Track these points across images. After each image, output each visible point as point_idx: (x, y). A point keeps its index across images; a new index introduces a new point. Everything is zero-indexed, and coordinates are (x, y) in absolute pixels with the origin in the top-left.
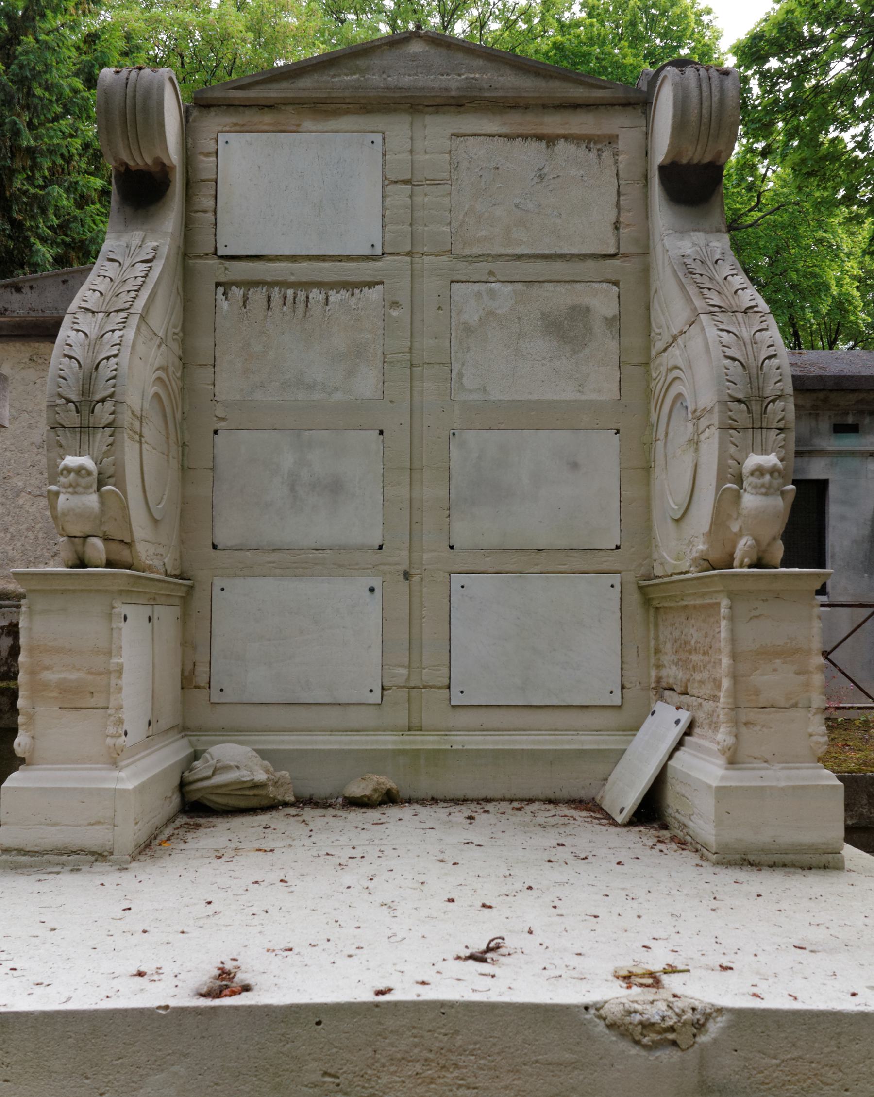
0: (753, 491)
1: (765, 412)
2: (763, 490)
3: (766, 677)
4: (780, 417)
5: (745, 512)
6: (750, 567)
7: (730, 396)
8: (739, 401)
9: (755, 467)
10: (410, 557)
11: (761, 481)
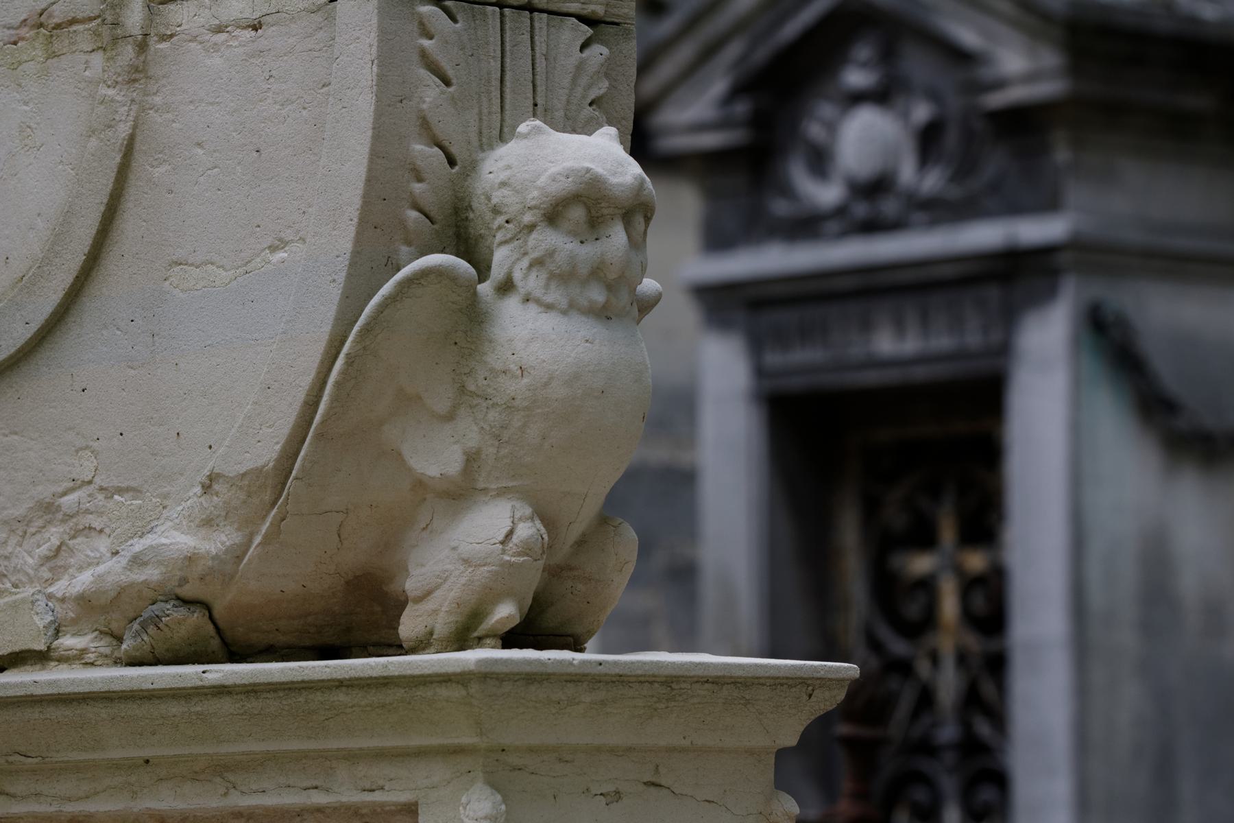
2: (597, 295)
5: (515, 387)
6: (510, 639)
9: (564, 187)
10: (211, 618)
11: (587, 252)
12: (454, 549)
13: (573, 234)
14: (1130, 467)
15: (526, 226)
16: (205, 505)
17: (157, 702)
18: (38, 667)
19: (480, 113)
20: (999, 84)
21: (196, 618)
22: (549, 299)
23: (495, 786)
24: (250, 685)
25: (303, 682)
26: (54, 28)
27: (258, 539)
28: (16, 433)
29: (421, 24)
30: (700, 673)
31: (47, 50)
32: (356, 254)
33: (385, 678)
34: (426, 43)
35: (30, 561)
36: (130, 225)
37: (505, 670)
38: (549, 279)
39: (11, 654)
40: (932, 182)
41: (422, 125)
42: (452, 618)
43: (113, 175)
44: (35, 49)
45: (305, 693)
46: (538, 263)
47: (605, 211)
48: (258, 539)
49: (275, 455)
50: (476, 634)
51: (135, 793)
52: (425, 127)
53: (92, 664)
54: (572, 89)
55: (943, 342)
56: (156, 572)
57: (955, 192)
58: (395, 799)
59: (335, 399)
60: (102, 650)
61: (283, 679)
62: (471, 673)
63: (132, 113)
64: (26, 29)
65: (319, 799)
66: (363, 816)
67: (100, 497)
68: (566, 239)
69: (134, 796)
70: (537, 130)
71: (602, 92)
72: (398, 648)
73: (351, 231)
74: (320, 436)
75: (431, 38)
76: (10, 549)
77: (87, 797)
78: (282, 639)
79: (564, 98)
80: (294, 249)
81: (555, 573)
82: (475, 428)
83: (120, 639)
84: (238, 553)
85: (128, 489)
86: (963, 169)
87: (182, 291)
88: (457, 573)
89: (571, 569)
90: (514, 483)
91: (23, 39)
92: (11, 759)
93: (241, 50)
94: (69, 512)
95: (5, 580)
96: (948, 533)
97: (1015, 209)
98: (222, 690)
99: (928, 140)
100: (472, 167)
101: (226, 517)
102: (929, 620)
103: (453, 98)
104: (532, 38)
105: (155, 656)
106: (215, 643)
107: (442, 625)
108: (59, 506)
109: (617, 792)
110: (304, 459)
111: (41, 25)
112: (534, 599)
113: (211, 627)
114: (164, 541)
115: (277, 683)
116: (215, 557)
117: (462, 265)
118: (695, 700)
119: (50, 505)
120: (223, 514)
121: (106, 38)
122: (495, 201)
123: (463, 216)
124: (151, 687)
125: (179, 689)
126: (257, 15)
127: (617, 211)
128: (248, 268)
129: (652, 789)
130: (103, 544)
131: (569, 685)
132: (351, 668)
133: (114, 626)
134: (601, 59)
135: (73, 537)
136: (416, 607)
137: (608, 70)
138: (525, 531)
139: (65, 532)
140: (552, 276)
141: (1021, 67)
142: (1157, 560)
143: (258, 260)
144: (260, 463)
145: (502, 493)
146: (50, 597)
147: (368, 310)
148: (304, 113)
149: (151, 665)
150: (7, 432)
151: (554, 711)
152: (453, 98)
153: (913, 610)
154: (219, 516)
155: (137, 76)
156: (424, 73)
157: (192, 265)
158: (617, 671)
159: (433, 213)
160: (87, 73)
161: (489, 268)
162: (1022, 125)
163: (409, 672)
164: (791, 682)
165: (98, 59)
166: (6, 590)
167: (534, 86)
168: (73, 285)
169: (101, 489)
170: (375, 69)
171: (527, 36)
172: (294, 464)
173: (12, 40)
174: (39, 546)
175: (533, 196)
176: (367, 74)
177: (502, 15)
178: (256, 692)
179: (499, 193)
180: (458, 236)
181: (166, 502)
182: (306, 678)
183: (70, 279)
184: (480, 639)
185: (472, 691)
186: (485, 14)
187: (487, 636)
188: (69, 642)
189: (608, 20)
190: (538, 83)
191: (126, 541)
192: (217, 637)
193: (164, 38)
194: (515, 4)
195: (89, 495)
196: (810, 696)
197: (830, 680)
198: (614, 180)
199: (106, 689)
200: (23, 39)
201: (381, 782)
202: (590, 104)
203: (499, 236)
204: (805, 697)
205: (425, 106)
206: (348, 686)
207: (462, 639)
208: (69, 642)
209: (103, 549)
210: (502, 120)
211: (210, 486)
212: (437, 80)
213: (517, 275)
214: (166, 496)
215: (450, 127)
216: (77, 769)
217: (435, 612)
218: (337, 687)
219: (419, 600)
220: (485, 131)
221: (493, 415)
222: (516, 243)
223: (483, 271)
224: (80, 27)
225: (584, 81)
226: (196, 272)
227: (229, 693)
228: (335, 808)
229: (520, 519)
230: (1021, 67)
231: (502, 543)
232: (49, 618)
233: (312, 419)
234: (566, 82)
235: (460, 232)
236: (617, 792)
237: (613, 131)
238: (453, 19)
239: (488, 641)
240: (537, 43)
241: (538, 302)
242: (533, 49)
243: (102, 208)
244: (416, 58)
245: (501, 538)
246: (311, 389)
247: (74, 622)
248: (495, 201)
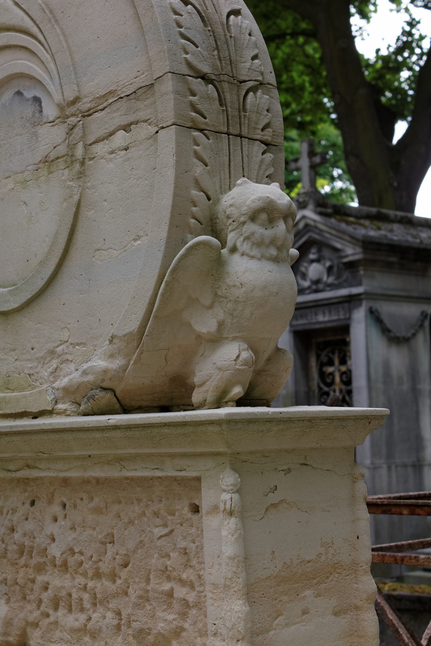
0: (255, 252)
1: (245, 110)
2: (273, 252)
3: (293, 628)
4: (266, 121)
5: (239, 292)
6: (240, 403)
7: (189, 64)
8: (204, 77)
9: (258, 204)
10: (115, 395)
11: (269, 233)
12: (214, 364)
13: (262, 225)
14: (379, 344)
15: (241, 223)
16: (110, 348)
17: (91, 432)
18: (49, 416)
19: (220, 179)
20: (347, 256)
21: (109, 396)
22: (252, 254)
23: (235, 470)
24: (127, 425)
25: (149, 424)
26: (51, 162)
27: (132, 362)
28: (40, 323)
29: (194, 140)
30: (324, 415)
31: (48, 171)
32: (169, 238)
33: (185, 422)
34: (196, 148)
35: (46, 374)
36: (80, 236)
37: (238, 418)
38: (252, 245)
39: (39, 411)
40: (331, 280)
41: (196, 183)
42: (214, 394)
43: (73, 216)
44: (44, 171)
45: (150, 429)
46: (247, 238)
47: (276, 215)
48: (132, 362)
49: (137, 326)
50: (225, 400)
51: (86, 469)
52: (197, 182)
53: (69, 415)
54: (259, 170)
55: (335, 317)
56: (92, 377)
57: (336, 282)
58: (191, 475)
59: (161, 301)
60: (73, 409)
61: (141, 423)
62: (222, 420)
63: (79, 191)
64: (41, 164)
65: (158, 474)
66: (178, 480)
67: (71, 347)
68: (259, 228)
69: (85, 470)
70: (245, 182)
71: (272, 172)
72: (190, 407)
73: (166, 228)
74: (156, 317)
75: (199, 146)
76: (39, 369)
77: (68, 470)
78: (144, 404)
79: (256, 174)
80: (143, 239)
81: (258, 373)
82: (222, 311)
83: (80, 405)
84: (124, 368)
85: (81, 344)
86: (338, 277)
87: (100, 261)
88: (216, 374)
89: (264, 371)
90: (240, 335)
91: (39, 168)
92: (38, 454)
93: (120, 159)
94: (59, 353)
95: (37, 382)
96: (337, 362)
97: (351, 286)
98: (116, 427)
99: (330, 270)
100: (218, 200)
101: (119, 353)
102: (333, 383)
103: (209, 172)
104: (242, 148)
105: (93, 412)
106: (117, 406)
107: (210, 397)
108: (56, 352)
109: (289, 469)
110: (149, 327)
111: (46, 162)
112: (249, 384)
113: (115, 399)
114: (95, 364)
115: (138, 424)
116: (115, 370)
117: (214, 240)
118: (322, 427)
119: (53, 351)
120: (118, 352)
121: (69, 162)
122: (228, 213)
123: (214, 222)
124: (88, 426)
125: (99, 427)
126: (127, 144)
128: (125, 249)
129: (304, 466)
130: (72, 366)
131: (267, 423)
132: (170, 417)
133: (78, 399)
134: (271, 159)
135: (61, 364)
136: (199, 389)
137: (273, 163)
138: (245, 355)
139: (58, 362)
140: (253, 244)
141: (352, 252)
142: (387, 366)
143: (129, 245)
144: (131, 330)
145: (234, 339)
146: (53, 388)
147: (174, 261)
148: (146, 181)
149: (92, 415)
150: (37, 323)
151: (261, 435)
152: (209, 172)
153: (329, 380)
154: (116, 353)
155: (81, 175)
156: (196, 160)
157: (103, 250)
158: (288, 416)
159: (202, 220)
160: (63, 178)
161: (226, 243)
162: (352, 266)
163: (195, 420)
164: (362, 417)
165: (66, 171)
166: (37, 386)
167: (243, 168)
168: (59, 262)
169: (71, 344)
170: (175, 158)
172: (145, 330)
173: (36, 169)
174: (49, 368)
175: (244, 209)
176: (171, 160)
177: (229, 138)
178: (130, 428)
179: (229, 210)
180: (212, 230)
181: (96, 348)
182: (150, 422)
183: (57, 260)
184: (226, 402)
185: (224, 428)
186: (221, 137)
187: (230, 401)
188: (61, 406)
189: (273, 144)
190: (245, 167)
191: (81, 365)
192: (118, 403)
193: (91, 159)
194: (234, 134)
195: (67, 347)
196: (370, 423)
197: (378, 416)
198: (279, 202)
199: (70, 427)
200: (39, 168)
201: (185, 467)
202: (267, 177)
203: (230, 228)
204: (368, 424)
205: (197, 175)
206: (168, 426)
207: (218, 403)
208: (61, 406)
209: (72, 368)
210: (230, 182)
211: (112, 341)
212: (201, 163)
213: (238, 244)
214: (95, 346)
215: (207, 183)
216: (63, 459)
217: (207, 391)
218: (164, 426)
219: (200, 386)
220: (223, 186)
221: (229, 305)
222: (237, 230)
223: (224, 245)
224: (60, 160)
225: (264, 167)
226: (105, 253)
227: (119, 428)
228: (166, 477)
229: (243, 350)
230: (352, 252)
231: (235, 360)
232: (53, 397)
233: (152, 310)
234: (256, 167)
235: (213, 227)
236: (289, 469)
237: (277, 184)
239: (230, 403)
240: (244, 150)
241: (248, 255)
242: (242, 153)
243: (69, 230)
244: (192, 154)
245: (234, 358)
246: (151, 297)
247: (62, 398)
248: (228, 213)
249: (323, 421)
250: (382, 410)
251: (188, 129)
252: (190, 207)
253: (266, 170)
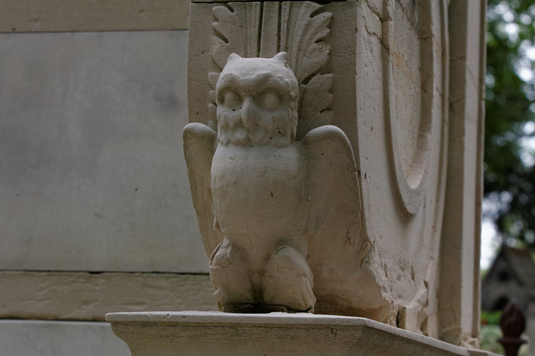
61: (435, 346)
75: (218, 21)
127: (246, 93)
131: (169, 327)
158: (195, 321)
171: (276, 14)
194: (207, 1)
225: (311, 31)
234: (300, 33)
238: (232, 10)
249: (255, 329)
250: (350, 319)
251: (209, 4)
252: (209, 90)
253: (315, 33)
